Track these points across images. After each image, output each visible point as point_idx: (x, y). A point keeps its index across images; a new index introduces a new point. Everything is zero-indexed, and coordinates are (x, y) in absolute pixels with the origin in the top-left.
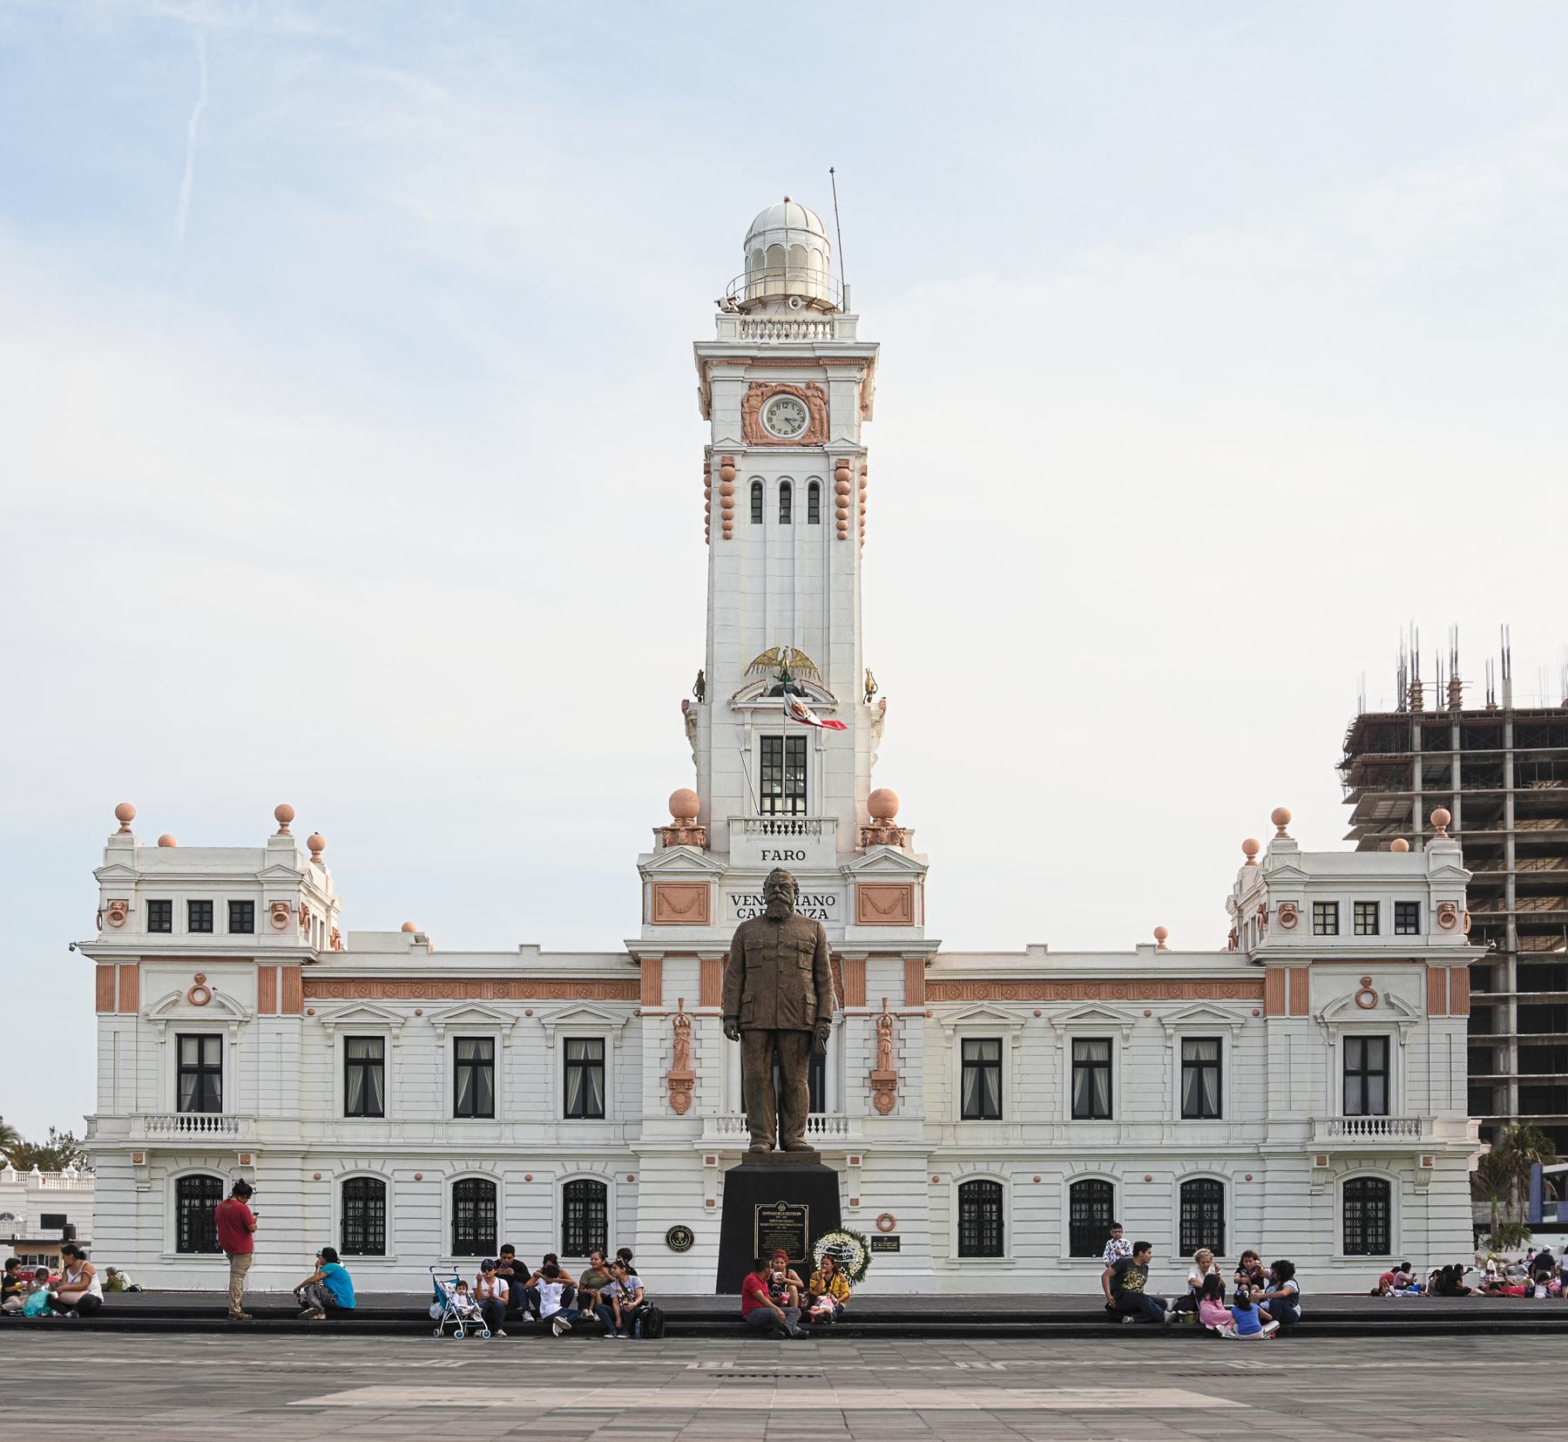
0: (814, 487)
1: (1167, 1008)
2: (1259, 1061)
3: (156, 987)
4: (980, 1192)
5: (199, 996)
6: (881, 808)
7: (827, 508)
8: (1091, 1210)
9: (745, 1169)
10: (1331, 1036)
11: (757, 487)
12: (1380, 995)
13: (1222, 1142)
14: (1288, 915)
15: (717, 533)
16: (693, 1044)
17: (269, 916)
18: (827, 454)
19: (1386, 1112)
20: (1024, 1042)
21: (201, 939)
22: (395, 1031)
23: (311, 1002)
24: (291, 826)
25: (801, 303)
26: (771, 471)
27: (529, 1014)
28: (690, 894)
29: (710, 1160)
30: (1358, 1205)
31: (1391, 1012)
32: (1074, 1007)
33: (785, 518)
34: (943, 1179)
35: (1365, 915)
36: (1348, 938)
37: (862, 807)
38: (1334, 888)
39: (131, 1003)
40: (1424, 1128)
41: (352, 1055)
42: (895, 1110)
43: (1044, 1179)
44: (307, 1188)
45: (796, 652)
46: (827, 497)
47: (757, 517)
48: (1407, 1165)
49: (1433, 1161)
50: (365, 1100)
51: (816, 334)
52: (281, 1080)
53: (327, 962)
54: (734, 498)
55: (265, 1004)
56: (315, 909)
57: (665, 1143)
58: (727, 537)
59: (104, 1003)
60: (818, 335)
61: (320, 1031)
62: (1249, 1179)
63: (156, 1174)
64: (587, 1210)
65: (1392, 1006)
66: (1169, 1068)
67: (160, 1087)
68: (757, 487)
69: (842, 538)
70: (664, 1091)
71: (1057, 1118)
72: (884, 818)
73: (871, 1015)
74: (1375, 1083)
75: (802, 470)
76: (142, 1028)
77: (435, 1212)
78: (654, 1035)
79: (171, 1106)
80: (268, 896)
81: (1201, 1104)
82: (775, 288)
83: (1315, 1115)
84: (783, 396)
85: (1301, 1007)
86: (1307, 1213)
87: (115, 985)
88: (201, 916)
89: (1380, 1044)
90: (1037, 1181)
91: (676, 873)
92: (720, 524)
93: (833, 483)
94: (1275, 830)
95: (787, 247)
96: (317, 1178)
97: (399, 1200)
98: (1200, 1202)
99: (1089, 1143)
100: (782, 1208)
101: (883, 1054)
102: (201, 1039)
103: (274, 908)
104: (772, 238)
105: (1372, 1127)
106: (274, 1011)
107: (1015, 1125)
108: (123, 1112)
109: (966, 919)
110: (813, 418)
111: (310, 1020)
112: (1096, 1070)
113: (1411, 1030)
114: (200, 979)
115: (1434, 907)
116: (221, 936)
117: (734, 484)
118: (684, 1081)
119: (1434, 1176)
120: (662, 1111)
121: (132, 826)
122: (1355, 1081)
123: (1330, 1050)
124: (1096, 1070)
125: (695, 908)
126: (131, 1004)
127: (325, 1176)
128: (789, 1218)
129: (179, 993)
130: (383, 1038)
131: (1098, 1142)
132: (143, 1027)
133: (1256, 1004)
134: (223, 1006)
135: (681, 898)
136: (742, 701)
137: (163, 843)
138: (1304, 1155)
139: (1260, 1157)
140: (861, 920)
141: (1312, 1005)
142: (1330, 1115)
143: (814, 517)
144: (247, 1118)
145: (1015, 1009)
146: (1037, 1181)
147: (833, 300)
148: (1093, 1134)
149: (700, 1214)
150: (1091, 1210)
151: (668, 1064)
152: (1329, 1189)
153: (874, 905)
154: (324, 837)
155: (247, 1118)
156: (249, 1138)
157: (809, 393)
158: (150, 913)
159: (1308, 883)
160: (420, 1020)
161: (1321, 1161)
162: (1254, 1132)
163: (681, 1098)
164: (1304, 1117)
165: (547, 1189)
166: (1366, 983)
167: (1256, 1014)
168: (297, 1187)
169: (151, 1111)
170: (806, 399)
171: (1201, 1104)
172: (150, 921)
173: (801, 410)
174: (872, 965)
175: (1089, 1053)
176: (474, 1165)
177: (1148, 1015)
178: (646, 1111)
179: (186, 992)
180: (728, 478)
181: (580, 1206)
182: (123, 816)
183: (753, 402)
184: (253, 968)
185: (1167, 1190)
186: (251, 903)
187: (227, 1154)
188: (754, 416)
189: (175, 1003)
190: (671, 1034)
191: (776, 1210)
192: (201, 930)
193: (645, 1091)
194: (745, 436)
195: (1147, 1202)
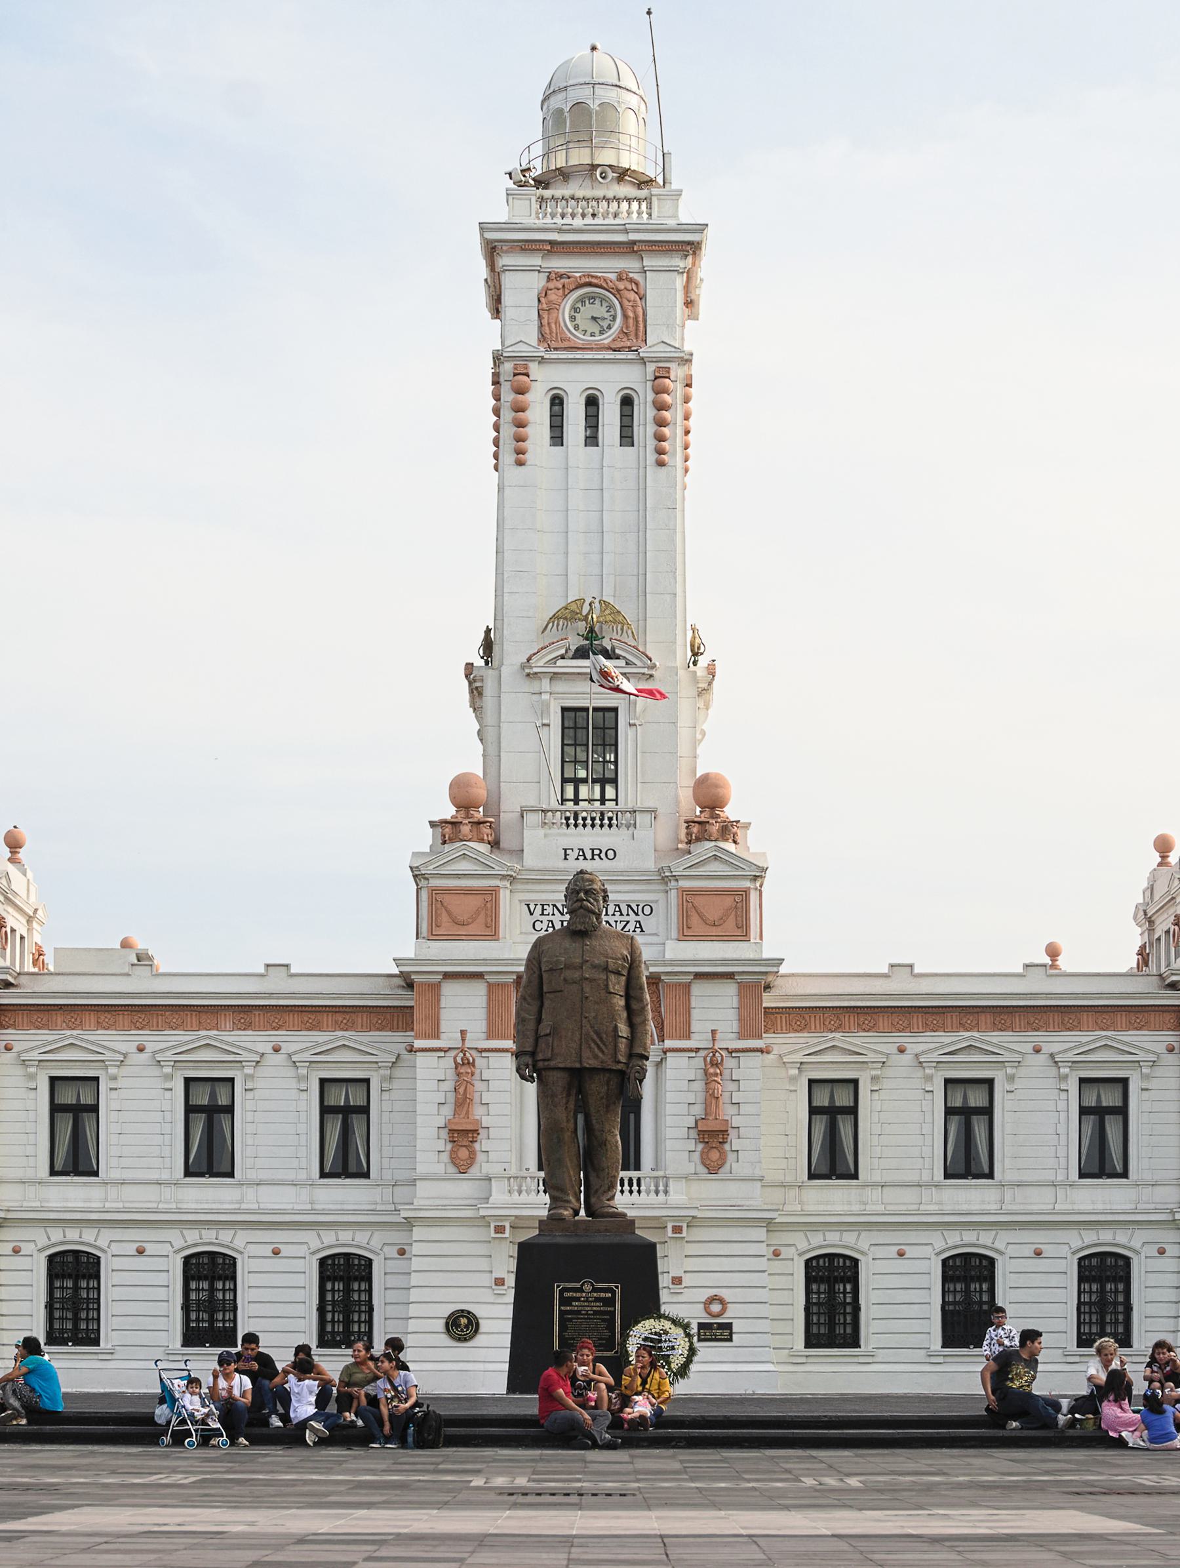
0: (627, 402)
1: (1060, 1042)
4: (831, 1268)
6: (710, 796)
9: (543, 1240)
11: (557, 402)
13: (1129, 1207)
15: (508, 458)
16: (479, 1086)
18: (643, 361)
20: (886, 1084)
25: (611, 175)
26: (575, 381)
27: (277, 1050)
28: (475, 902)
29: (500, 1229)
32: (947, 1040)
33: (592, 440)
34: (786, 1252)
37: (686, 795)
42: (727, 1167)
43: (910, 1252)
46: (644, 413)
54: (529, 415)
57: (444, 1208)
58: (520, 463)
60: (632, 214)
61: (19, 1071)
62: (1162, 1252)
64: (348, 1291)
66: (1063, 1115)
68: (557, 402)
69: (661, 464)
70: (443, 1144)
71: (926, 1177)
72: (713, 808)
73: (697, 1050)
75: (612, 379)
77: (161, 1294)
78: (431, 1075)
81: (1102, 1161)
82: (580, 157)
90: (901, 1254)
92: (511, 446)
93: (651, 396)
95: (594, 106)
96: (16, 1251)
97: (117, 1278)
99: (965, 1208)
101: (712, 1098)
104: (575, 95)
107: (874, 1185)
109: (811, 935)
110: (625, 317)
112: (1107, 1117)
118: (466, 1132)
120: (439, 1169)
127: (27, 1248)
128: (597, 1300)
131: (975, 1207)
135: (464, 907)
136: (539, 665)
140: (685, 933)
143: (627, 438)
145: (874, 1044)
146: (901, 1254)
148: (970, 1197)
149: (487, 1295)
150: (967, 1291)
151: (448, 1111)
154: (25, 832)
157: (621, 286)
163: (463, 1153)
165: (299, 1265)
170: (617, 293)
171: (1102, 1161)
173: (611, 307)
174: (698, 989)
177: (1037, 1051)
178: (421, 1169)
181: (339, 1286)
183: (552, 296)
185: (1061, 1265)
188: (554, 314)
190: (451, 1074)
191: (581, 1290)
194: (542, 338)
195: (1037, 1280)
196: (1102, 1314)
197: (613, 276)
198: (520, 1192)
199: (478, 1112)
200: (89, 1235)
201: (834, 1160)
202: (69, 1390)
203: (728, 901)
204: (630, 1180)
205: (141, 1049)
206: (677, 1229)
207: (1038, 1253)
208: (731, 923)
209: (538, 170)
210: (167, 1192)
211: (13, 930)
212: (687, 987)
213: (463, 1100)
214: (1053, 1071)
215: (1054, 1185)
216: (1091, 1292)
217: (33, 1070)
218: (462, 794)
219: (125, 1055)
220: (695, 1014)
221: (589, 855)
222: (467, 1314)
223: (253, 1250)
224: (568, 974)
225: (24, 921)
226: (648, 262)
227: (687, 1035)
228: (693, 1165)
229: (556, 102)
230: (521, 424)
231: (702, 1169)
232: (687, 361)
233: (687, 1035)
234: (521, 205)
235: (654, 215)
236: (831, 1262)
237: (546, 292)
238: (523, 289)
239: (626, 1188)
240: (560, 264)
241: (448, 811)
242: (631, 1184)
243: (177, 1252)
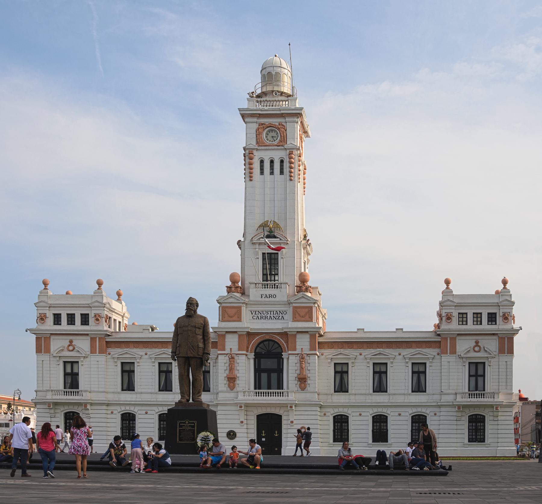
0: (282, 162)
1: (407, 352)
2: (439, 371)
3: (56, 344)
4: (342, 418)
5: (71, 348)
6: (303, 279)
7: (286, 170)
8: (380, 425)
9: (176, 408)
10: (464, 362)
11: (262, 162)
12: (482, 347)
13: (426, 401)
14: (449, 318)
15: (248, 179)
16: (236, 365)
17: (94, 319)
18: (286, 149)
19: (484, 390)
20: (356, 364)
21: (71, 327)
22: (138, 360)
23: (110, 350)
24: (102, 287)
25: (278, 93)
26: (267, 156)
27: (146, 354)
28: (234, 311)
29: (241, 407)
30: (474, 424)
31: (485, 353)
32: (373, 351)
33: (272, 173)
34: (327, 414)
35: (477, 317)
36: (470, 326)
37: (297, 278)
38: (465, 308)
39: (48, 350)
40: (496, 396)
41: (124, 369)
42: (306, 389)
43: (363, 414)
44: (109, 416)
45: (274, 222)
46: (286, 165)
47: (262, 173)
48: (491, 410)
49: (499, 408)
50: (128, 385)
51: (285, 105)
52: (99, 376)
53: (115, 335)
54: (253, 166)
55: (93, 351)
56: (114, 316)
57: (226, 400)
58: (251, 180)
59: (39, 350)
60: (284, 105)
61: (112, 360)
62: (435, 414)
63: (57, 411)
64: (341, 426)
65: (486, 351)
66: (407, 374)
67: (58, 380)
68: (262, 162)
69: (291, 180)
71: (367, 392)
72: (304, 282)
73: (298, 354)
74: (480, 379)
75: (277, 155)
76: (52, 359)
77: (152, 425)
79: (61, 387)
80: (93, 312)
81: (419, 387)
82: (269, 88)
83: (458, 391)
84: (272, 129)
85: (453, 351)
86: (455, 427)
87: (42, 343)
88: (71, 319)
89: (482, 365)
90: (360, 415)
91: (230, 303)
92: (249, 176)
93: (288, 160)
94: (445, 286)
95: (274, 73)
96: (112, 413)
97: (140, 421)
98: (419, 423)
99: (379, 401)
100: (187, 422)
101: (302, 368)
102: (72, 363)
103: (95, 316)
104: (268, 70)
105: (477, 396)
106: (96, 353)
107: (352, 394)
108: (45, 389)
109: (333, 321)
110: (281, 136)
111: (109, 356)
112: (421, 374)
113: (492, 360)
114: (71, 342)
115: (501, 315)
116: (78, 326)
117: (253, 161)
118: (232, 378)
119: (500, 414)
120: (225, 389)
121: (48, 287)
122: (473, 379)
123: (464, 367)
124: (421, 374)
125: (307, 316)
126: (48, 351)
127: (115, 412)
128: (190, 426)
129: (64, 347)
130: (134, 363)
131: (382, 401)
132: (52, 359)
133: (437, 350)
134: (79, 351)
135: (232, 312)
136: (255, 240)
137: (67, 293)
138: (453, 406)
139: (439, 406)
140: (295, 320)
141: (457, 350)
142: (464, 391)
143: (282, 172)
144: (86, 391)
145: (352, 353)
146: (360, 415)
147: (290, 92)
148: (381, 398)
149: (238, 426)
150: (380, 425)
151: (227, 372)
152: (463, 418)
153: (299, 314)
154: (122, 292)
155: (86, 391)
156: (86, 398)
157: (280, 127)
158: (54, 318)
159: (456, 306)
160: (147, 356)
161: (459, 408)
162: (436, 397)
163: (232, 384)
164: (454, 392)
166: (477, 342)
167: (438, 354)
168: (105, 416)
169: (55, 389)
170: (279, 129)
171: (419, 387)
172: (54, 321)
173: (277, 133)
174: (298, 336)
175: (380, 369)
176: (380, 410)
177: (400, 354)
178: (220, 389)
179: (66, 346)
180: (251, 159)
181: (339, 424)
182: (45, 283)
183: (260, 130)
184: (89, 338)
185: (406, 418)
186: (88, 314)
187: (79, 404)
188: (261, 136)
189: (62, 350)
190: (228, 361)
191: (185, 423)
192: (71, 324)
193: (220, 382)
194: (257, 143)
195: (399, 423)
196: (476, 432)
197: (277, 124)
200: (132, 408)
201: (341, 387)
203: (307, 310)
204: (259, 393)
205: (146, 354)
207: (400, 415)
208: (307, 316)
209: (259, 91)
210: (154, 396)
211: (115, 320)
212: (295, 336)
213: (231, 369)
214: (404, 361)
215: (404, 394)
216: (473, 426)
218: (233, 278)
219: (142, 356)
220: (298, 344)
221: (268, 296)
222: (233, 432)
223: (354, 414)
224: (184, 328)
225: (121, 317)
226: (287, 119)
227: (295, 350)
229: (263, 72)
230: (251, 169)
231: (299, 389)
233: (295, 350)
234: (251, 103)
235: (290, 105)
236: (341, 417)
237: (258, 129)
240: (262, 120)
241: (229, 284)
242: (268, 394)
243: (157, 413)
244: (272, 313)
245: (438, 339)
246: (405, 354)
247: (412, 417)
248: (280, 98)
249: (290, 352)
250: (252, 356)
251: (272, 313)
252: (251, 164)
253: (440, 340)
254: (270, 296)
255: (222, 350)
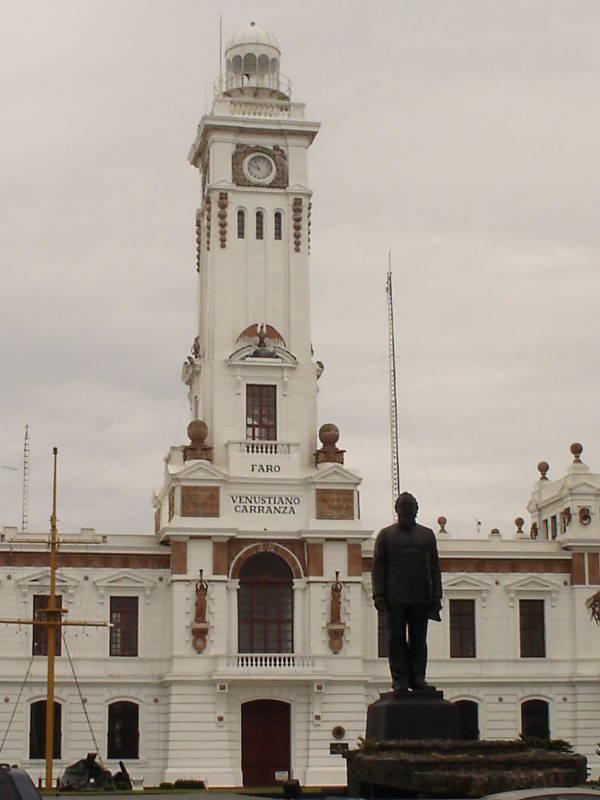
0: (278, 216)
11: (241, 214)
18: (287, 194)
22: (70, 591)
27: (9, 577)
29: (223, 688)
54: (228, 220)
68: (241, 214)
73: (326, 582)
78: (183, 597)
94: (573, 457)
133: (566, 577)
136: (236, 361)
143: (278, 235)
146: (501, 700)
163: (200, 643)
170: (274, 157)
183: (239, 156)
194: (234, 180)
198: (303, 665)
199: (208, 617)
202: (212, 786)
206: (319, 688)
212: (185, 544)
217: (26, 590)
227: (184, 571)
228: (189, 650)
232: (309, 196)
233: (184, 571)
238: (221, 153)
239: (259, 662)
244: (272, 501)
245: (166, 551)
246: (19, 576)
247: (110, 706)
248: (269, 101)
249: (312, 578)
250: (235, 584)
251: (272, 501)
252: (298, 220)
253: (569, 558)
254: (269, 468)
255: (180, 573)
